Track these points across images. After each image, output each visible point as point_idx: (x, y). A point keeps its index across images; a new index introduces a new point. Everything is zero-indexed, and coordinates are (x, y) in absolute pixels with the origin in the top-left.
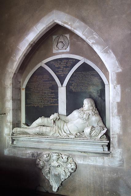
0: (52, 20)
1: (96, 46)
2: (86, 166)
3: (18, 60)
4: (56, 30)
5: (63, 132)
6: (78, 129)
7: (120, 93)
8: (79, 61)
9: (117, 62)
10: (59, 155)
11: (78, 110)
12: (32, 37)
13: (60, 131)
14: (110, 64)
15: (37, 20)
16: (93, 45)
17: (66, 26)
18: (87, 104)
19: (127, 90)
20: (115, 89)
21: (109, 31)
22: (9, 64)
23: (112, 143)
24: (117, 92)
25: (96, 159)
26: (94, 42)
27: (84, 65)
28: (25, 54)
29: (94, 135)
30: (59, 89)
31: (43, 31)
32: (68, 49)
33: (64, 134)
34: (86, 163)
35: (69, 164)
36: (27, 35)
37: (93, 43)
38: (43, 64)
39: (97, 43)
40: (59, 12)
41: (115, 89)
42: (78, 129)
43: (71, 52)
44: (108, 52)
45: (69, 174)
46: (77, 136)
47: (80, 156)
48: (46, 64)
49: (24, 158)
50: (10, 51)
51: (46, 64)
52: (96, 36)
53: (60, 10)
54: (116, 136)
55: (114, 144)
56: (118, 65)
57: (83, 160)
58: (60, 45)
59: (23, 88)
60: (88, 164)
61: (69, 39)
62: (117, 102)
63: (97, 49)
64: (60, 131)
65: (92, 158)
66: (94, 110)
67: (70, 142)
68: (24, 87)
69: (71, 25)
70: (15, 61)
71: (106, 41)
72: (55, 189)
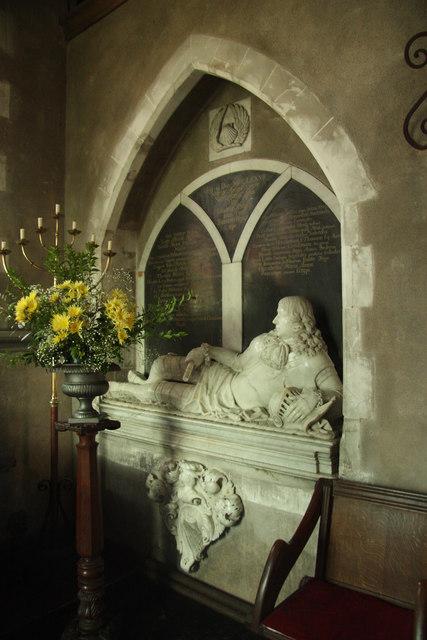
0: (185, 67)
1: (300, 121)
2: (260, 507)
3: (111, 192)
4: (206, 95)
5: (215, 402)
6: (258, 396)
7: (371, 276)
8: (274, 176)
9: (361, 167)
10: (197, 470)
11: (265, 335)
12: (142, 123)
13: (207, 399)
14: (344, 180)
15: (149, 76)
16: (291, 120)
17: (221, 74)
18: (287, 316)
19: (394, 263)
20: (356, 260)
21: (348, 62)
22: (95, 207)
23: (345, 450)
24: (363, 273)
25: (295, 496)
26: (294, 108)
27: (293, 187)
28: (129, 174)
29: (291, 416)
30: (225, 268)
31: (166, 102)
32: (248, 145)
33: (217, 407)
34: (270, 505)
35: (221, 501)
36: (131, 120)
37: (290, 114)
38: (183, 197)
39: (303, 111)
40: (204, 36)
41: (356, 260)
42: (258, 396)
43: (254, 154)
44: (335, 134)
45: (219, 530)
46: (247, 418)
47: (255, 482)
48: (194, 196)
49: (124, 467)
50: (97, 172)
51: (194, 196)
52: (298, 89)
53: (205, 33)
54: (358, 426)
55: (351, 452)
56: (363, 174)
57: (262, 496)
58: (226, 134)
59: (140, 270)
60: (275, 510)
61: (249, 114)
62: (362, 306)
63: (303, 130)
64: (207, 399)
65: (286, 492)
66: (305, 337)
67: (227, 434)
68: (142, 267)
69: (231, 70)
70: (106, 197)
71: (327, 99)
72: (186, 563)
